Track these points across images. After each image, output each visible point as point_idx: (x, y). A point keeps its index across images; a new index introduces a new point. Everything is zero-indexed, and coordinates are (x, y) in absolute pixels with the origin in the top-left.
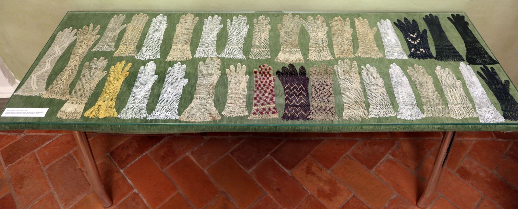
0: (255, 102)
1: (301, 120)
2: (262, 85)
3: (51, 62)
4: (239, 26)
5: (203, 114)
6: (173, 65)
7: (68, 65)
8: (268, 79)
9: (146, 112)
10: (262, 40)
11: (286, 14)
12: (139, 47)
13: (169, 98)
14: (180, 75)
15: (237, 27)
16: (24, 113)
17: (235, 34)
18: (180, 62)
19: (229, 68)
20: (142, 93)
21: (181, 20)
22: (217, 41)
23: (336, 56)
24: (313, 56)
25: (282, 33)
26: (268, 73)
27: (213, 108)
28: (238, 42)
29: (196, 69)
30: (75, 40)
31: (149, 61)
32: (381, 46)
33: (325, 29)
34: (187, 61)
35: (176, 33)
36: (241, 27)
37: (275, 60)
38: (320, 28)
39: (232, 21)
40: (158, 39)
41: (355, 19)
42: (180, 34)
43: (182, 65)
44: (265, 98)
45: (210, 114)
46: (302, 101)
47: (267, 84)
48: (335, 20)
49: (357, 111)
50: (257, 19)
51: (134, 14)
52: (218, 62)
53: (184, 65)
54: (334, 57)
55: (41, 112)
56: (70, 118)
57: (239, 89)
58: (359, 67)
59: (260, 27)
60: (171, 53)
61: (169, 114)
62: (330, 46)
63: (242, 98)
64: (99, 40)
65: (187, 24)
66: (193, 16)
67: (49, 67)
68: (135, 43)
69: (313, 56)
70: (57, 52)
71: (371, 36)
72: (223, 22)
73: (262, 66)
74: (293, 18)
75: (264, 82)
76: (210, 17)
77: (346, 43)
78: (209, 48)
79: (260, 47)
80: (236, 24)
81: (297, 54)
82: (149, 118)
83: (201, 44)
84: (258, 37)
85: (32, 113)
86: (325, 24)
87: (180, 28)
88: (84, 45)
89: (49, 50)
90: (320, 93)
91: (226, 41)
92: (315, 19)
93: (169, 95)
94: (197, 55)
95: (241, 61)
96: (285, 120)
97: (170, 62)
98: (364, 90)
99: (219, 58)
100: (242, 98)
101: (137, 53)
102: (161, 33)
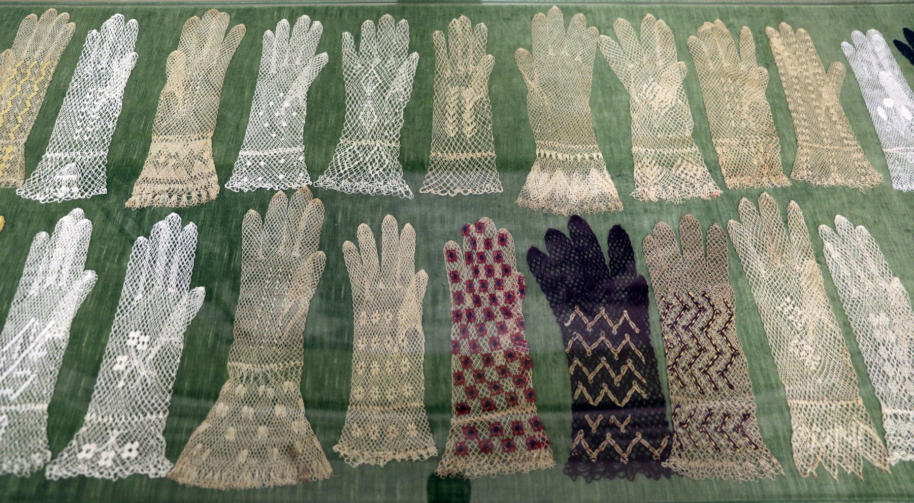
0: (458, 395)
2: (479, 314)
4: (384, 58)
5: (259, 453)
6: (153, 222)
8: (499, 284)
9: (42, 441)
10: (467, 116)
11: (541, 9)
12: (34, 151)
14: (174, 268)
15: (377, 60)
17: (369, 90)
19: (353, 238)
20: (36, 354)
21: (185, 36)
22: (309, 119)
23: (731, 182)
24: (651, 185)
25: (533, 85)
26: (498, 257)
27: (300, 426)
28: (381, 124)
29: (234, 242)
31: (66, 207)
32: (868, 138)
33: (676, 70)
34: (201, 206)
35: (168, 88)
36: (392, 61)
37: (520, 200)
38: (660, 63)
39: (357, 39)
40: (104, 114)
41: (769, 29)
42: (179, 95)
43: (184, 224)
44: (495, 377)
45: (290, 451)
46: (636, 387)
47: (496, 310)
48: (706, 35)
49: (839, 432)
50: (445, 29)
51: (24, 13)
52: (312, 213)
53: (191, 227)
54: (723, 186)
57: (394, 335)
58: (814, 226)
59: (454, 63)
60: (144, 174)
61: (134, 454)
62: (703, 136)
63: (410, 378)
65: (205, 51)
66: (226, 18)
68: (21, 130)
69: (651, 185)
71: (829, 97)
72: (329, 43)
73: (472, 228)
74: (566, 26)
75: (485, 297)
76: (284, 22)
77: (753, 125)
78: (281, 150)
79: (459, 143)
80: (375, 48)
81: (594, 173)
82: (56, 472)
83: (250, 131)
84: (452, 101)
86: (672, 51)
87: (181, 67)
90: (712, 352)
91: (341, 120)
92: (637, 29)
93: (136, 363)
94: (239, 183)
95: (393, 204)
96: (581, 481)
97: (142, 210)
98: (846, 325)
99: (315, 192)
100: (410, 378)
101: (27, 175)
102: (114, 92)
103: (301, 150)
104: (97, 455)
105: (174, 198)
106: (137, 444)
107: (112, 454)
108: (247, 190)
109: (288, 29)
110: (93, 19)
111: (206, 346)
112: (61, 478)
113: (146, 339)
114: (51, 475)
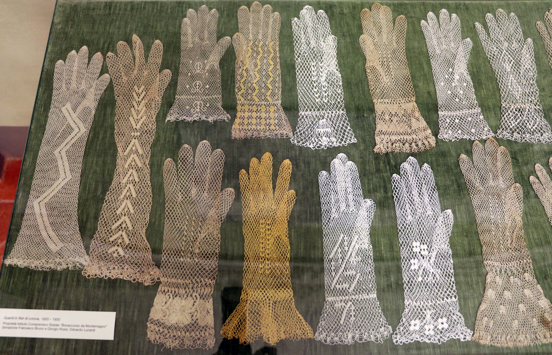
1: (352, 286)
3: (69, 157)
7: (119, 169)
9: (383, 320)
13: (425, 273)
16: (37, 327)
18: (413, 155)
19: (259, 159)
21: (364, 23)
30: (110, 88)
31: (333, 152)
34: (426, 151)
55: (101, 325)
56: (187, 343)
64: (173, 85)
67: (69, 177)
70: (73, 125)
85: (76, 328)
88: (139, 103)
89: (49, 121)
99: (500, 141)
103: (479, 111)
104: (422, 327)
105: (407, 145)
106: (445, 320)
107: (432, 327)
108: (453, 140)
109: (435, 18)
110: (294, 10)
111: (465, 250)
112: (109, 278)
113: (425, 247)
114: (397, 342)
